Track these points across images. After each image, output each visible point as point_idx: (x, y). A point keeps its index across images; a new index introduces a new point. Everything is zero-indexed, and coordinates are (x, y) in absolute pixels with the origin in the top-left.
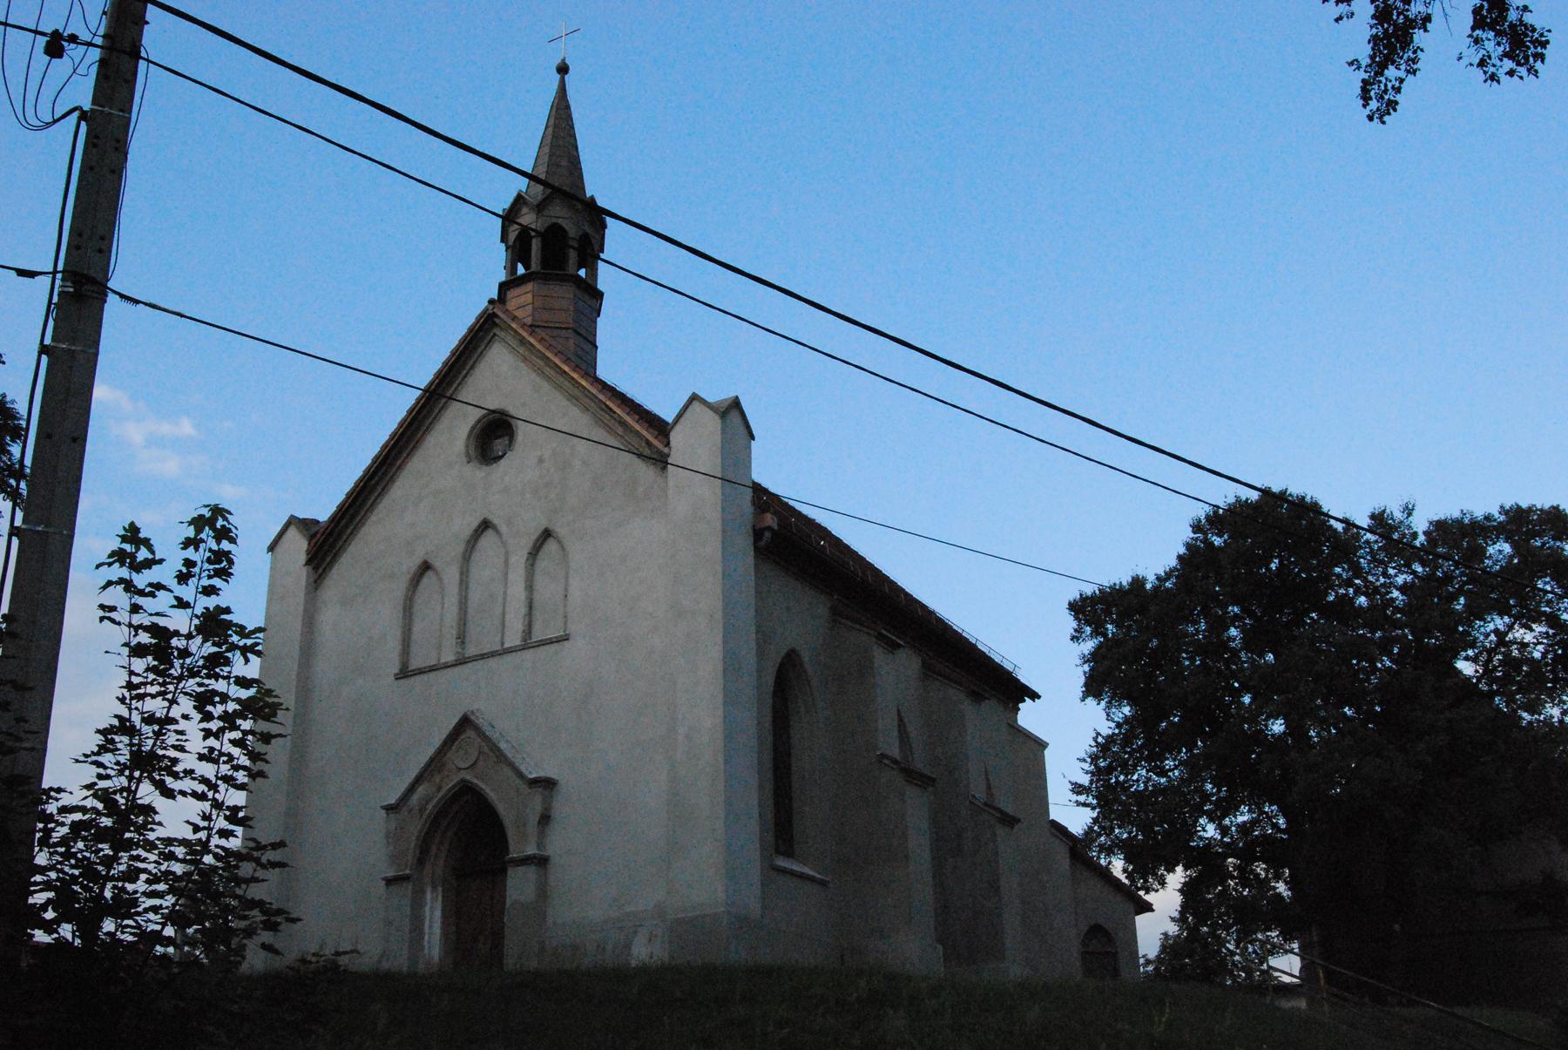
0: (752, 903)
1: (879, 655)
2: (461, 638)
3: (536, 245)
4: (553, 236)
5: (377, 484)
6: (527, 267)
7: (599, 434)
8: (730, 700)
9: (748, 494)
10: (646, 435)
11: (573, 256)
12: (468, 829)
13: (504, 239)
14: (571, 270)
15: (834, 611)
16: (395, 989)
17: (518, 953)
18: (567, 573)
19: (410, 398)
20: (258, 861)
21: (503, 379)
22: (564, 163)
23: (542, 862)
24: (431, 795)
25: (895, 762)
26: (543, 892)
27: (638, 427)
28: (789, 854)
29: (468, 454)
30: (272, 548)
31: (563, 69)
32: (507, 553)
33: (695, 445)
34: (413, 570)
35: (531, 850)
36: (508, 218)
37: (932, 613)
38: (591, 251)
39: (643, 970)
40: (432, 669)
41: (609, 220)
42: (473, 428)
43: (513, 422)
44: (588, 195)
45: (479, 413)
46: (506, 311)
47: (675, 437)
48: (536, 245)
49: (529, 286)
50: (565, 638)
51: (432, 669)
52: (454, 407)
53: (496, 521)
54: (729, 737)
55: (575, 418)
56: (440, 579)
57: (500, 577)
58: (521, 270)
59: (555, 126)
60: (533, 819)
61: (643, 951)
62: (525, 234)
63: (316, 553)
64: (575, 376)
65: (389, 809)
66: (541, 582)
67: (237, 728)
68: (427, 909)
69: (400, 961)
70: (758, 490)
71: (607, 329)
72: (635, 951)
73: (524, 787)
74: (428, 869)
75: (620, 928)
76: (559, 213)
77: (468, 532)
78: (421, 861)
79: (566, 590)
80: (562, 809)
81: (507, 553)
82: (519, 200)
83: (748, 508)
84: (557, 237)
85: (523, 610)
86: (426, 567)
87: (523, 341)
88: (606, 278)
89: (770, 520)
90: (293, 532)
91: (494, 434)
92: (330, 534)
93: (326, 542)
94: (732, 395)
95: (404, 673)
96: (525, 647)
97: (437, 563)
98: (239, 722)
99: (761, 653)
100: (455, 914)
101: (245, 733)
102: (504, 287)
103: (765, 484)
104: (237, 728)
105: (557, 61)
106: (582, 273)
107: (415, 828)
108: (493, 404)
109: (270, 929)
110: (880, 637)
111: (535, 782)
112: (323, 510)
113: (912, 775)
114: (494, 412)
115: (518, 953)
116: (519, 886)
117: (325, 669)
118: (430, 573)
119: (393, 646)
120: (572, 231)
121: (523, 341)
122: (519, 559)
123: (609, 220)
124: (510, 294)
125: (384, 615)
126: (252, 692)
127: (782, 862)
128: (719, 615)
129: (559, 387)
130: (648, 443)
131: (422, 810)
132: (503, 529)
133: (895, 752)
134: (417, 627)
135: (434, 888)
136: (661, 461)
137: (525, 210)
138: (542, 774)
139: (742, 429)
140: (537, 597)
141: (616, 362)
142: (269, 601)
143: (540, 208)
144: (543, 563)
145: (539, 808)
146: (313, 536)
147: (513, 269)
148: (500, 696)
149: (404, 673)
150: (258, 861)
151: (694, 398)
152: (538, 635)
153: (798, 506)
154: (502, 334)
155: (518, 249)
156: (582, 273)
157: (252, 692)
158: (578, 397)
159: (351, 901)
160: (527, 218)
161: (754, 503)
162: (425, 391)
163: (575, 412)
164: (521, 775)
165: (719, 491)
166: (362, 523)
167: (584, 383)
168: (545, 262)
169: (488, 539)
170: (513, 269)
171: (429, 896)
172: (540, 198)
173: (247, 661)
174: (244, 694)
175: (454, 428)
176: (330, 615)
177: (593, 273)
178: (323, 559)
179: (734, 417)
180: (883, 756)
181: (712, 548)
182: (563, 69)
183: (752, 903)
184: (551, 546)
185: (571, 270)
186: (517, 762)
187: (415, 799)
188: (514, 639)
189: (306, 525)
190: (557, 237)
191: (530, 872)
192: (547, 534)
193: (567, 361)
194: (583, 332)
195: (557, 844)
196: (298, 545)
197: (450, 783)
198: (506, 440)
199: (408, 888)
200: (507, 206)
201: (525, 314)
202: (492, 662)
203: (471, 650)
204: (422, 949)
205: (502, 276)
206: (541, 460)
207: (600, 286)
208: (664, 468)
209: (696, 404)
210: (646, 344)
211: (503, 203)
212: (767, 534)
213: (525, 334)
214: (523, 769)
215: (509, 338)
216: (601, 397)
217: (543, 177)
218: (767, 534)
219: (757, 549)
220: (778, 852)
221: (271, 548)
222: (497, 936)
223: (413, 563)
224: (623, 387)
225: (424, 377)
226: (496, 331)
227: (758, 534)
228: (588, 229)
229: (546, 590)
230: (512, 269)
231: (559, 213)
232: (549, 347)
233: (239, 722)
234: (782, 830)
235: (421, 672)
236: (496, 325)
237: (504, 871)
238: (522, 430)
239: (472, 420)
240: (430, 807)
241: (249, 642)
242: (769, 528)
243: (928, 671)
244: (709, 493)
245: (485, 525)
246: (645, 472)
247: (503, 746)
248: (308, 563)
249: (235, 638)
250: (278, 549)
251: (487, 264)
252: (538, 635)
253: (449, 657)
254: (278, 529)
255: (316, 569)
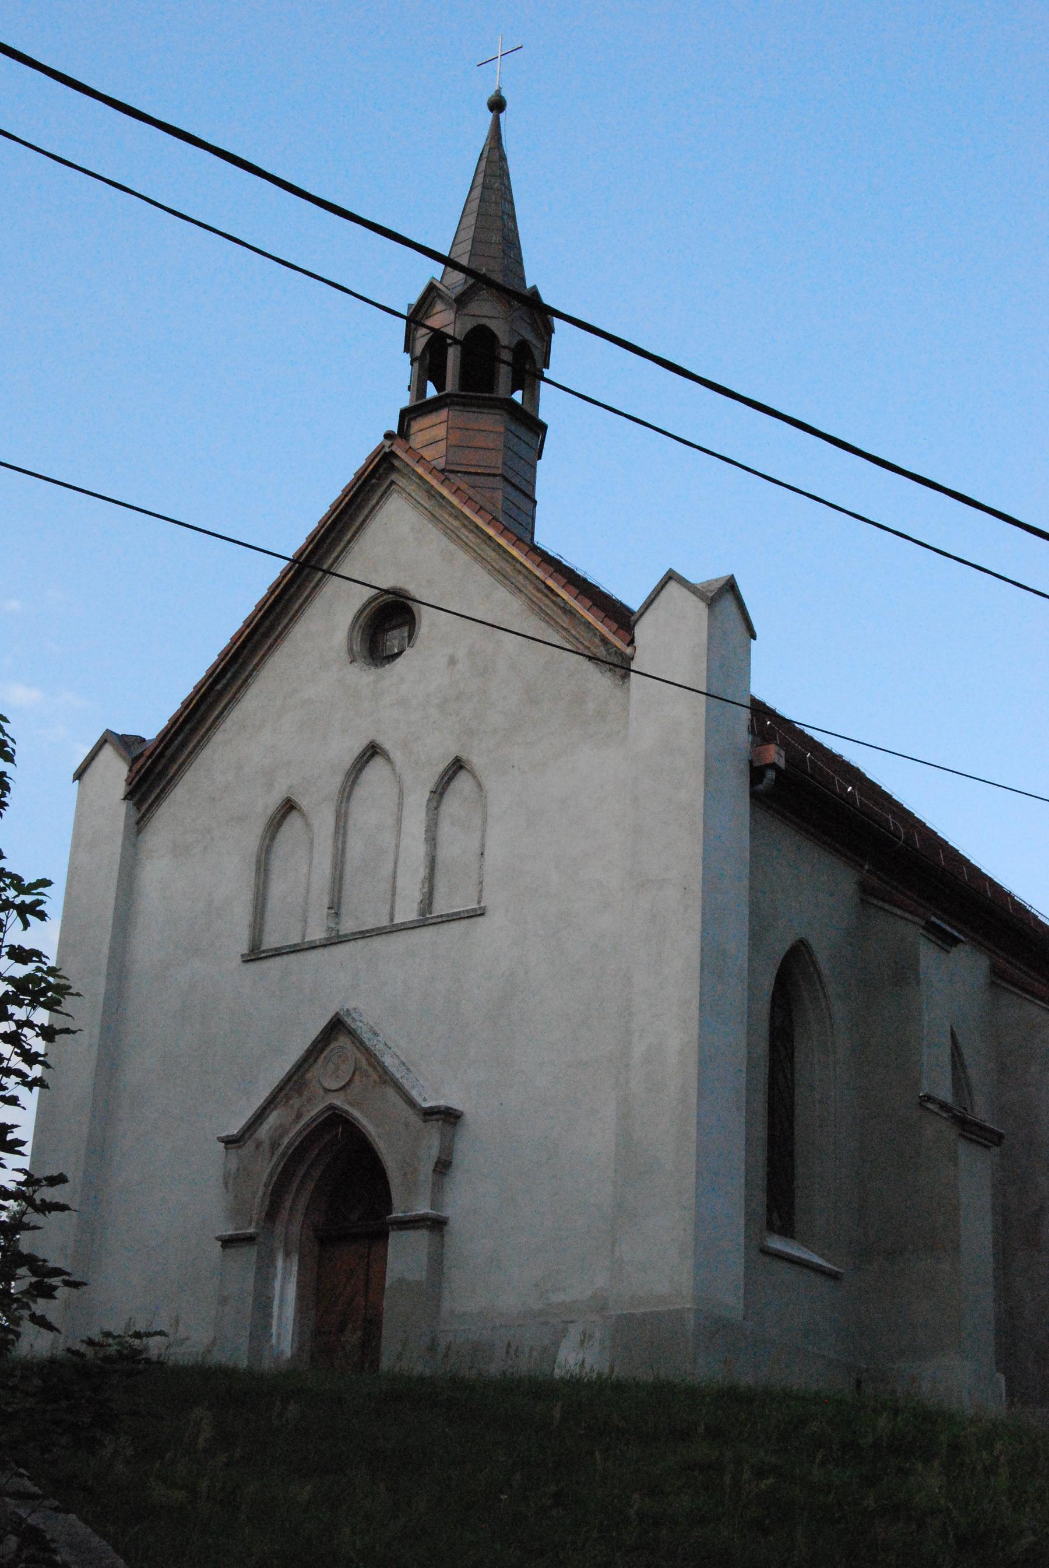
0: (731, 1300)
1: (928, 955)
2: (335, 909)
3: (453, 356)
4: (479, 343)
5: (225, 688)
6: (440, 387)
7: (534, 626)
8: (709, 1007)
9: (745, 714)
10: (601, 625)
11: (504, 374)
12: (337, 1177)
13: (408, 348)
14: (501, 392)
15: (865, 890)
16: (222, 1390)
17: (400, 1352)
18: (485, 821)
19: (273, 570)
20: (30, 1201)
21: (402, 547)
22: (496, 238)
23: (437, 1225)
24: (287, 1125)
25: (943, 1106)
26: (437, 1263)
27: (590, 617)
28: (787, 1231)
29: (350, 650)
30: (79, 775)
31: (497, 105)
32: (401, 792)
33: (669, 643)
34: (270, 812)
35: (423, 1208)
36: (415, 318)
37: (1009, 895)
38: (530, 366)
39: (574, 1383)
40: (295, 950)
41: (557, 322)
42: (361, 612)
43: (415, 607)
44: (529, 285)
45: (369, 593)
46: (409, 450)
47: (642, 632)
48: (453, 356)
49: (443, 414)
50: (479, 913)
51: (295, 950)
52: (333, 584)
53: (387, 745)
54: (704, 1062)
55: (505, 604)
56: (308, 825)
57: (390, 820)
58: (431, 391)
59: (485, 187)
60: (426, 1169)
61: (574, 1358)
62: (438, 341)
63: (139, 784)
64: (491, 532)
65: (230, 1142)
66: (446, 830)
67: (9, 1017)
68: (277, 1284)
69: (236, 1354)
70: (759, 710)
71: (551, 477)
72: (561, 1357)
73: (415, 1119)
74: (279, 1229)
75: (546, 1323)
76: (487, 311)
77: (348, 760)
78: (271, 1215)
79: (483, 846)
80: (467, 1153)
81: (401, 792)
82: (432, 292)
83: (743, 737)
84: (483, 350)
85: (422, 872)
86: (289, 807)
87: (431, 493)
88: (551, 405)
89: (774, 754)
90: (108, 751)
91: (388, 621)
92: (161, 755)
93: (152, 770)
94: (730, 574)
95: (255, 954)
96: (422, 923)
97: (303, 802)
98: (12, 1009)
99: (756, 938)
100: (316, 1295)
101: (20, 1024)
102: (407, 416)
103: (771, 703)
104: (9, 1017)
105: (489, 94)
106: (518, 396)
107: (264, 1169)
108: (387, 581)
109: (43, 1296)
110: (932, 929)
111: (430, 1114)
112: (150, 724)
113: (971, 1130)
114: (387, 592)
115: (400, 1352)
116: (404, 1257)
117: (148, 947)
118: (294, 816)
119: (241, 913)
120: (504, 338)
121: (431, 493)
122: (418, 799)
123: (557, 322)
124: (416, 426)
125: (229, 875)
126: (30, 968)
127: (777, 1243)
128: (697, 887)
129: (482, 560)
130: (604, 641)
131: (274, 1145)
132: (396, 755)
133: (945, 1093)
134: (277, 889)
135: (287, 1255)
136: (621, 666)
137: (439, 306)
138: (442, 1103)
139: (741, 627)
140: (444, 854)
141: (562, 525)
142: (76, 846)
143: (461, 301)
144: (452, 804)
145: (435, 1152)
146: (135, 760)
147: (421, 391)
148: (389, 991)
149: (255, 954)
150: (30, 1201)
151: (671, 576)
152: (441, 907)
153: (818, 737)
154: (402, 482)
155: (429, 362)
156: (518, 396)
157: (30, 968)
158: (507, 573)
159: (173, 1269)
160: (442, 318)
161: (751, 731)
162: (294, 561)
163: (502, 593)
164: (411, 1103)
165: (702, 710)
166: (199, 746)
167: (515, 552)
168: (466, 379)
169: (376, 769)
170: (421, 391)
171: (280, 1263)
172: (459, 290)
173: (26, 925)
174: (20, 971)
175: (334, 613)
176: (157, 870)
177: (533, 397)
178: (150, 791)
179: (728, 604)
180: (929, 1098)
181: (691, 790)
182: (497, 105)
183: (731, 1300)
184: (463, 783)
185: (501, 392)
186: (407, 1084)
187: (264, 1131)
188: (408, 912)
189: (126, 744)
190: (483, 350)
191: (420, 1238)
192: (457, 766)
193: (493, 521)
194: (516, 480)
195: (465, 1200)
196: (115, 771)
197: (314, 1111)
198: (405, 631)
199: (249, 1255)
200: (414, 299)
201: (436, 455)
202: (377, 943)
203: (348, 926)
204: (269, 1340)
205: (405, 400)
206: (452, 661)
207: (543, 416)
208: (625, 677)
209: (672, 587)
210: (603, 499)
211: (407, 297)
212: (771, 775)
213: (434, 482)
214: (414, 1093)
215: (411, 488)
216: (538, 573)
217: (464, 261)
218: (771, 775)
219: (754, 796)
220: (771, 1227)
221: (79, 775)
222: (372, 1326)
223: (274, 800)
224: (572, 560)
225: (293, 541)
226: (394, 477)
227: (756, 773)
228: (529, 336)
229: (455, 844)
230: (420, 391)
231: (487, 311)
232: (468, 501)
233: (12, 1009)
234: (779, 1194)
235: (278, 953)
236: (393, 468)
237: (382, 1236)
238: (426, 618)
239: (357, 604)
240: (286, 1141)
241: (28, 899)
242: (773, 766)
243: (998, 978)
244: (689, 714)
245: (372, 751)
246: (598, 681)
247: (388, 1061)
248: (129, 796)
249: (11, 893)
250: (86, 776)
251: (381, 382)
252: (441, 907)
253: (317, 933)
254: (87, 750)
255: (138, 805)
